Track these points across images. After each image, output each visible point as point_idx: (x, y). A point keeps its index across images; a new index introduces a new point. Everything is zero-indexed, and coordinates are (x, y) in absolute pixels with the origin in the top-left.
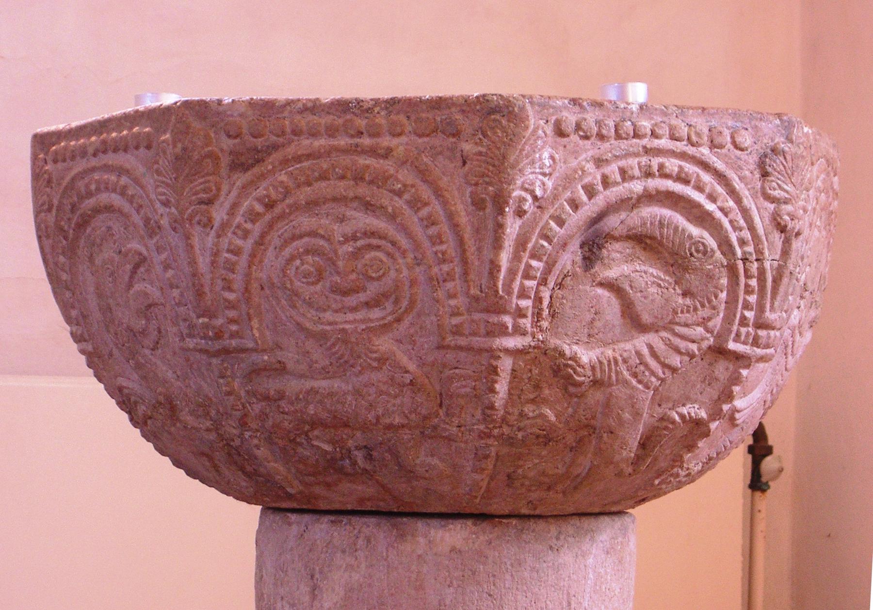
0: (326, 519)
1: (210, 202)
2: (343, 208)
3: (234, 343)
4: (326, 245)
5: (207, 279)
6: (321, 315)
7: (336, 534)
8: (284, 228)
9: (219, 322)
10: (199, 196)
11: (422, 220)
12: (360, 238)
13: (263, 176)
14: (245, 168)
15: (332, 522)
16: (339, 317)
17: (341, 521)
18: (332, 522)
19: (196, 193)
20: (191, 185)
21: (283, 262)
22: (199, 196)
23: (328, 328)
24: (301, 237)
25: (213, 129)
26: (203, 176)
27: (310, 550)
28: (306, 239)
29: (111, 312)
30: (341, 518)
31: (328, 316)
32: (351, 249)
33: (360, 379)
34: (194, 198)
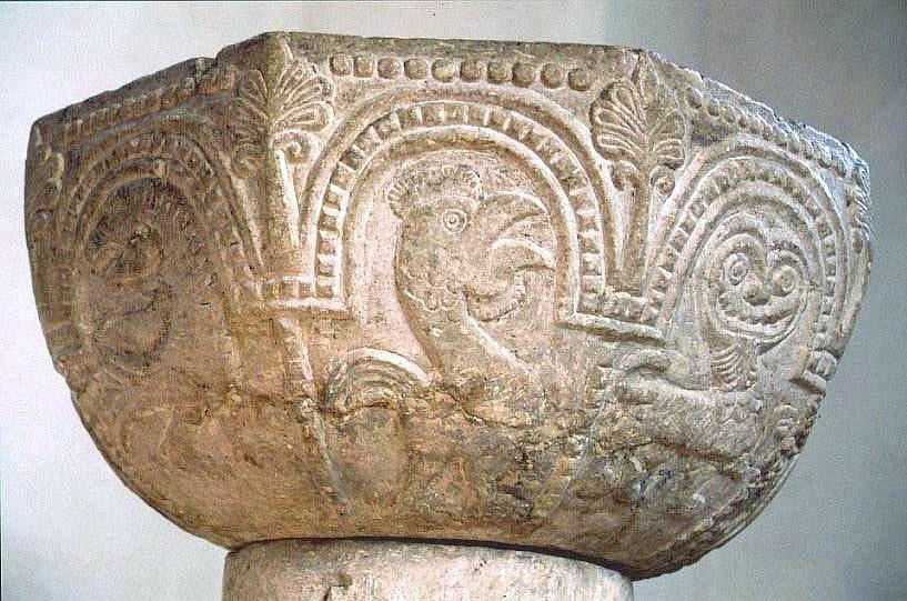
0: (512, 554)
1: (675, 166)
2: (774, 214)
3: (644, 328)
4: (760, 246)
5: (650, 250)
6: (729, 318)
7: (525, 571)
8: (732, 217)
9: (642, 301)
10: (668, 156)
11: (827, 246)
12: (785, 249)
13: (721, 157)
14: (704, 143)
15: (519, 556)
16: (746, 326)
17: (530, 557)
18: (519, 556)
19: (666, 153)
20: (662, 142)
21: (724, 253)
22: (668, 156)
23: (733, 334)
24: (744, 231)
25: (676, 92)
26: (673, 137)
27: (491, 588)
28: (746, 235)
29: (396, 283)
30: (528, 554)
31: (735, 320)
32: (776, 257)
33: (726, 397)
34: (663, 156)
